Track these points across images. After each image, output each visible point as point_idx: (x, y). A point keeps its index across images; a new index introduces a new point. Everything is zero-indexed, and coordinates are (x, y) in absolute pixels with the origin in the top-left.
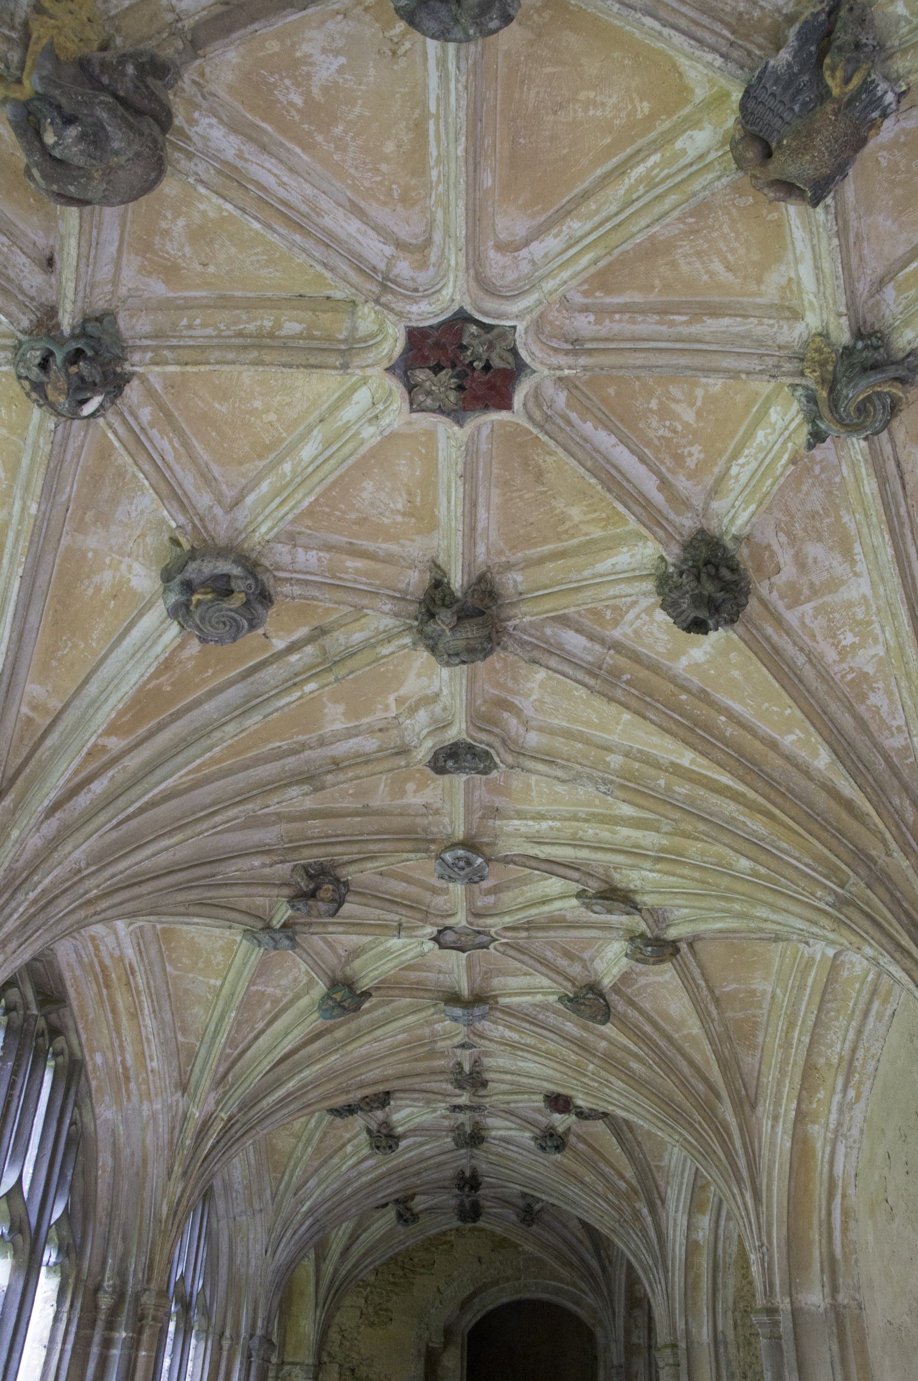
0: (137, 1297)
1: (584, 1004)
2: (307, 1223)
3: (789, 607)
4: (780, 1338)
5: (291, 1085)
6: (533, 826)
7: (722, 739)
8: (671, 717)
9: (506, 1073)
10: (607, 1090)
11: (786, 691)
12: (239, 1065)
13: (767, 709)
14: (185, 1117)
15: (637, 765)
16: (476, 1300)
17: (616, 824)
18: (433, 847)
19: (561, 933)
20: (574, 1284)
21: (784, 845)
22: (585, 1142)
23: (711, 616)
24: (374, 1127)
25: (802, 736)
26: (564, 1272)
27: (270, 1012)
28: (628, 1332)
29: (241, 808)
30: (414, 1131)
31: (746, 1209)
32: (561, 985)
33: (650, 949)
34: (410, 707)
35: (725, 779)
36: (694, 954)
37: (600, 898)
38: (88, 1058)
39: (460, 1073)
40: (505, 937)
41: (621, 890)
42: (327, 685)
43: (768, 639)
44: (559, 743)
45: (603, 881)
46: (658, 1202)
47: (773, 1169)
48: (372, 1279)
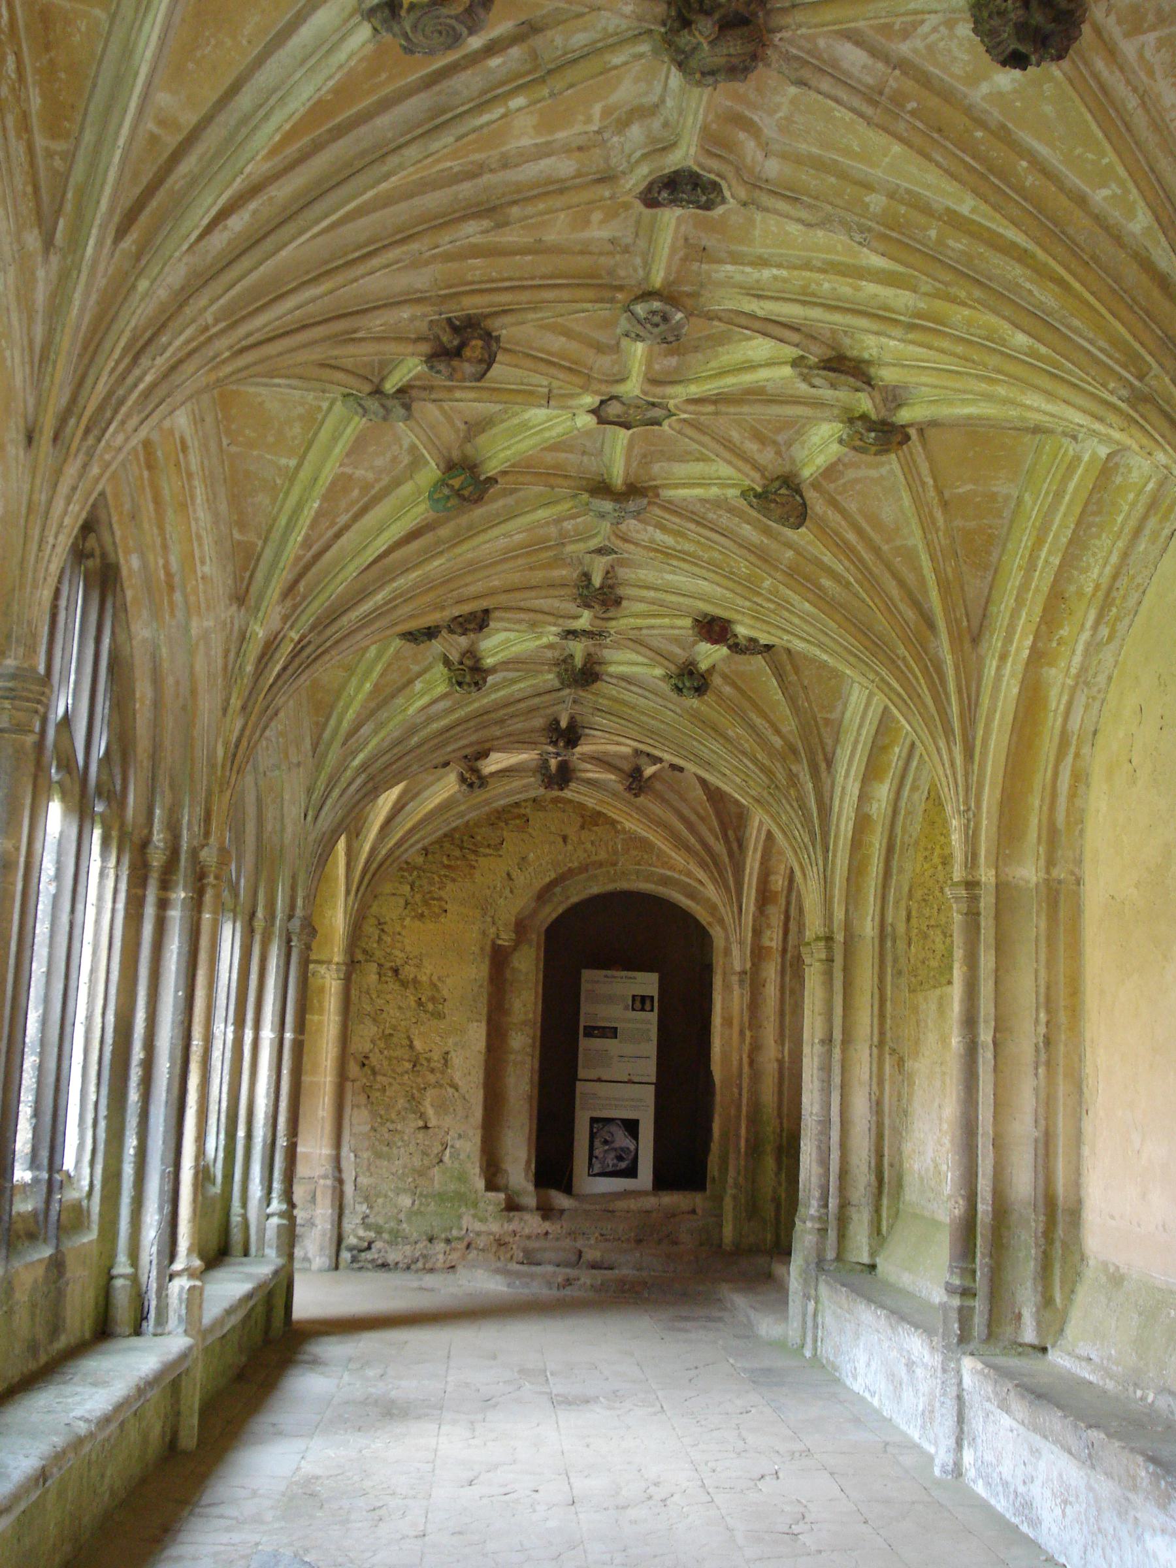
0: (194, 853)
1: (775, 501)
2: (359, 781)
3: (1127, 35)
4: (978, 914)
5: (379, 597)
6: (752, 274)
7: (1020, 190)
8: (963, 161)
9: (648, 588)
10: (786, 614)
11: (1111, 143)
12: (314, 570)
13: (1079, 156)
14: (243, 637)
15: (903, 209)
16: (558, 890)
17: (861, 277)
18: (619, 296)
19: (758, 409)
20: (689, 874)
21: (1076, 323)
22: (734, 685)
23: (1035, 51)
24: (454, 656)
25: (1119, 191)
26: (678, 858)
27: (358, 501)
28: (757, 933)
29: (405, 248)
30: (505, 664)
31: (953, 764)
32: (747, 476)
33: (873, 435)
34: (619, 120)
35: (1012, 234)
36: (924, 443)
37: (824, 368)
38: (122, 561)
39: (587, 587)
40: (685, 412)
41: (850, 360)
42: (540, 101)
43: (1096, 76)
44: (807, 178)
45: (828, 346)
46: (823, 766)
47: (992, 720)
48: (420, 860)
